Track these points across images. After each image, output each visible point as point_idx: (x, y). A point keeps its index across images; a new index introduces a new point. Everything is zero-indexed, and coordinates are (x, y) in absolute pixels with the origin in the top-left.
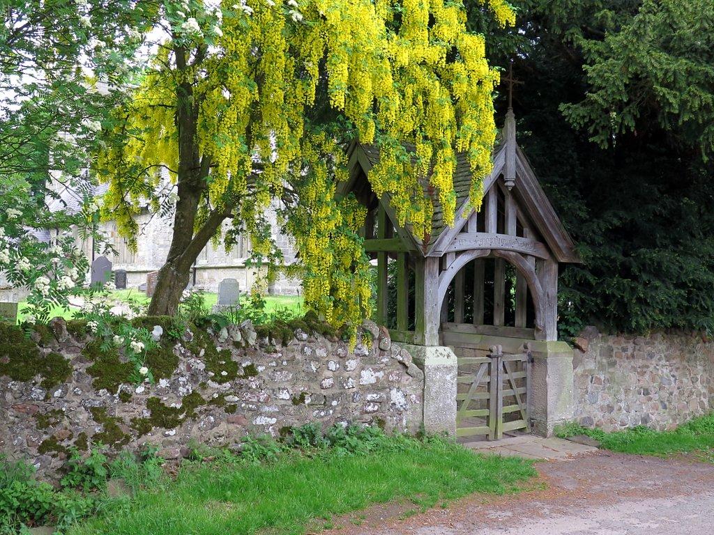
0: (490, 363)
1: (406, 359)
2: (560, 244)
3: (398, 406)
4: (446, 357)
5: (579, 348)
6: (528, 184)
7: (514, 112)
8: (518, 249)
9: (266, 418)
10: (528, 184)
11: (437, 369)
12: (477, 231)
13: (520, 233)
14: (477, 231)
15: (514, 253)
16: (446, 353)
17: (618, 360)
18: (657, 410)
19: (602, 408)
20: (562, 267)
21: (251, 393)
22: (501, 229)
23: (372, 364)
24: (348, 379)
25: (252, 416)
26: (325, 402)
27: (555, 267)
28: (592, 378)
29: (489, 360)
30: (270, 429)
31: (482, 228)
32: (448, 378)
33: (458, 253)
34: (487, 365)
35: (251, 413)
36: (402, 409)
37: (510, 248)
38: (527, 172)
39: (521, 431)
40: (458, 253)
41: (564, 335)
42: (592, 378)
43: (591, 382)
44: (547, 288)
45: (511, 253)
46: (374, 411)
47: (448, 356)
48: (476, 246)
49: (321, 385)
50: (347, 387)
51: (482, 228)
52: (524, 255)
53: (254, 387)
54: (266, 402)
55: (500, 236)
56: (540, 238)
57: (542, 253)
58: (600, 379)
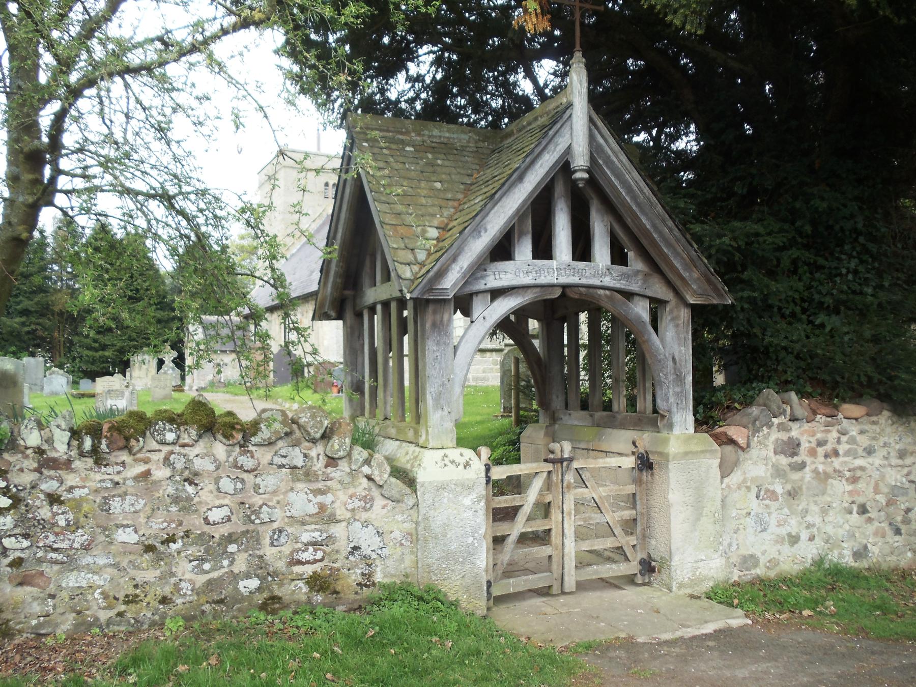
0: (549, 472)
1: (376, 472)
2: (686, 275)
3: (366, 551)
4: (461, 467)
5: (732, 442)
6: (619, 176)
7: (583, 56)
8: (612, 285)
9: (91, 575)
10: (619, 176)
11: (442, 487)
12: (534, 258)
13: (618, 257)
14: (534, 258)
15: (607, 292)
16: (462, 461)
17: (808, 460)
18: (884, 537)
19: (780, 540)
20: (697, 312)
21: (57, 534)
22: (582, 250)
23: (310, 481)
24: (261, 507)
25: (60, 572)
26: (213, 548)
27: (685, 314)
28: (759, 491)
29: (550, 467)
30: (96, 595)
31: (543, 250)
32: (467, 501)
33: (496, 294)
34: (545, 474)
35: (56, 568)
36: (374, 556)
37: (596, 282)
38: (617, 157)
39: (631, 580)
40: (496, 294)
41: (709, 412)
42: (759, 491)
43: (758, 497)
44: (673, 344)
45: (601, 292)
46: (316, 561)
47: (467, 465)
48: (528, 280)
49: (206, 519)
50: (257, 521)
51: (543, 250)
52: (629, 295)
53: (62, 523)
54: (86, 548)
55: (581, 265)
56: (655, 266)
57: (659, 290)
58: (773, 492)
